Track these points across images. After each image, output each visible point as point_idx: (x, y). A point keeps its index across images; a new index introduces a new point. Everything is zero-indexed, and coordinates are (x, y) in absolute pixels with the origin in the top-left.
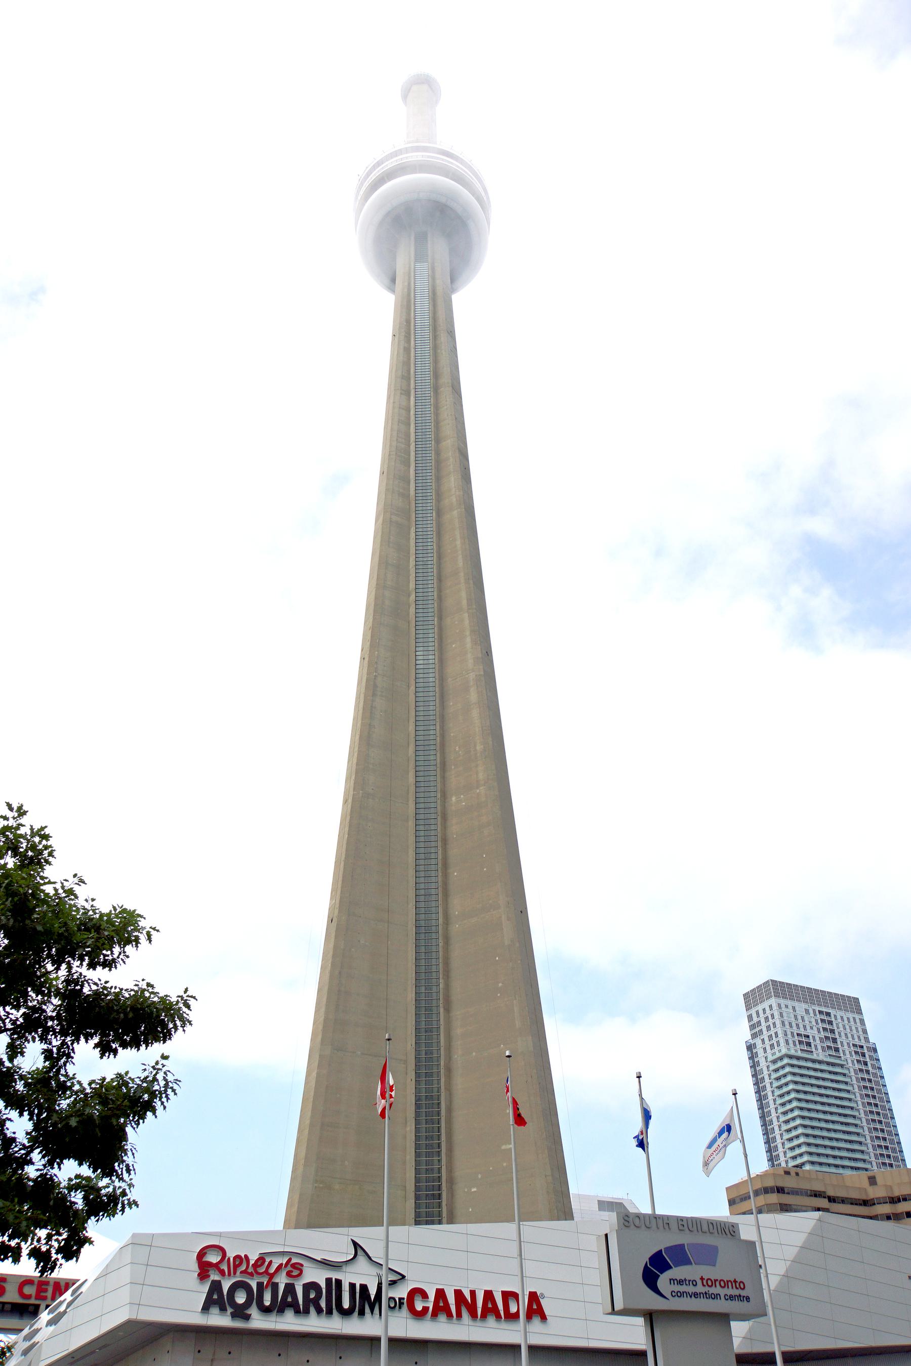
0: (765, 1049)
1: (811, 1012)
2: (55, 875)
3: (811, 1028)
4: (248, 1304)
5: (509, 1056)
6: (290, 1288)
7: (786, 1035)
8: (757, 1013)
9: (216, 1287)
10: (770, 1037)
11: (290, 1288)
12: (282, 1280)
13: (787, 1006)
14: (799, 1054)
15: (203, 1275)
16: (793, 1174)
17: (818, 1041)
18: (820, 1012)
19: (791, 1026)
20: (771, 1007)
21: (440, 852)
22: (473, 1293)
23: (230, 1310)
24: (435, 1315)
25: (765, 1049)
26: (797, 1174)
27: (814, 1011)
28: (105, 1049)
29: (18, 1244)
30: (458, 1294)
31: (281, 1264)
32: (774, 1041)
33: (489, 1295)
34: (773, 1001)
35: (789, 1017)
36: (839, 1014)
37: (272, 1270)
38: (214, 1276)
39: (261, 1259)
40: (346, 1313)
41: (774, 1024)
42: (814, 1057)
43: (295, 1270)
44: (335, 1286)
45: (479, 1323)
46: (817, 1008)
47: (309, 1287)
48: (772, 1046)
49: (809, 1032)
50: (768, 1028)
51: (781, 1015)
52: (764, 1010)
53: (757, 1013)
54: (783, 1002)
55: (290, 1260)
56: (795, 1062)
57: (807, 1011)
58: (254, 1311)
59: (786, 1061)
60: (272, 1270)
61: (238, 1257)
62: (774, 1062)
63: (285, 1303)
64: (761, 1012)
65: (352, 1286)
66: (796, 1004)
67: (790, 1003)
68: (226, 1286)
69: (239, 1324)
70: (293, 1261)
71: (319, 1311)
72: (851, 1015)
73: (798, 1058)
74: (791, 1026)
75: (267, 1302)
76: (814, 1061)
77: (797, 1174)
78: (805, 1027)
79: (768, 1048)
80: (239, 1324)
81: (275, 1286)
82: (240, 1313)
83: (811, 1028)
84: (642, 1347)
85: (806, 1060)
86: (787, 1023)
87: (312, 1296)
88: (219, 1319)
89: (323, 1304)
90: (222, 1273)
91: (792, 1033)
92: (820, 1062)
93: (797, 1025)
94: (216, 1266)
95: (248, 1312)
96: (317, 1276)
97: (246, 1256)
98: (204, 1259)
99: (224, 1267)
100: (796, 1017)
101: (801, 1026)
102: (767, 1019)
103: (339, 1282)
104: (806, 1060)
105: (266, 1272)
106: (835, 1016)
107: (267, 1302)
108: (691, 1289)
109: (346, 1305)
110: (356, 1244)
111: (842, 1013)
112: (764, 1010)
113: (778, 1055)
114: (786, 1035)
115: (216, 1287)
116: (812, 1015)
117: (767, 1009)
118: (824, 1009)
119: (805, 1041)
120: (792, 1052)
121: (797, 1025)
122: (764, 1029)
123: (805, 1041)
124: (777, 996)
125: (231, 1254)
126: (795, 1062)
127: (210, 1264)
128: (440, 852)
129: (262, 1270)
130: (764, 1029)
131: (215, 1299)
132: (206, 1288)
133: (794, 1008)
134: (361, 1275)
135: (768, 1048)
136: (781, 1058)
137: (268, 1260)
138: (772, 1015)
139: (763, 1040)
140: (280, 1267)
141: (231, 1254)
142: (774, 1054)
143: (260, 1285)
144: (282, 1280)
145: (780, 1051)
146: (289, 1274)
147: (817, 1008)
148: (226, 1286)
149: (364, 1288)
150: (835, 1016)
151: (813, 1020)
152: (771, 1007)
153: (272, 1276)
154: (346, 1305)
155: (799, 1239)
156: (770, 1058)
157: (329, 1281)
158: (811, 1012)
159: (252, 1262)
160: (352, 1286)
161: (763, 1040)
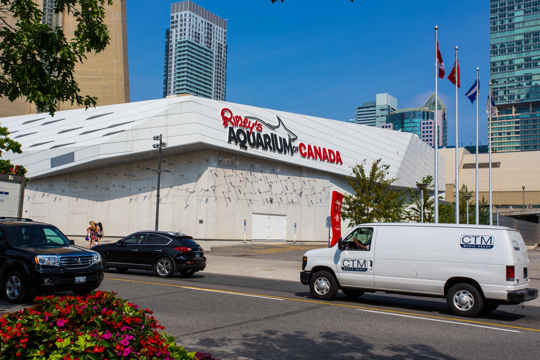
0: (176, 36)
1: (204, 22)
3: (202, 30)
5: (456, 49)
7: (190, 31)
8: (177, 16)
10: (181, 30)
11: (259, 135)
13: (193, 17)
14: (193, 42)
15: (226, 125)
17: (203, 38)
18: (208, 24)
19: (193, 27)
20: (185, 15)
22: (319, 148)
25: (176, 36)
27: (205, 22)
32: (183, 32)
34: (188, 12)
35: (193, 22)
36: (216, 27)
40: (280, 151)
41: (185, 24)
42: (200, 45)
44: (274, 136)
45: (322, 162)
46: (207, 21)
48: (181, 35)
49: (200, 32)
50: (181, 25)
51: (190, 20)
52: (181, 15)
53: (177, 16)
54: (192, 14)
55: (256, 122)
56: (190, 45)
57: (202, 21)
59: (187, 44)
61: (237, 116)
62: (180, 43)
63: (256, 144)
64: (179, 16)
66: (198, 17)
67: (195, 15)
68: (235, 130)
69: (242, 150)
70: (258, 122)
72: (221, 29)
73: (193, 44)
74: (193, 27)
76: (199, 47)
78: (199, 29)
79: (179, 35)
80: (242, 150)
81: (253, 133)
82: (243, 145)
83: (202, 30)
84: (76, 159)
85: (196, 45)
86: (191, 25)
87: (267, 141)
88: (235, 147)
91: (193, 31)
92: (202, 48)
93: (196, 27)
99: (233, 120)
100: (196, 23)
101: (198, 28)
102: (182, 20)
103: (275, 136)
104: (196, 45)
106: (214, 27)
111: (218, 27)
112: (181, 15)
113: (183, 40)
114: (190, 31)
116: (204, 24)
117: (183, 15)
118: (210, 23)
119: (197, 36)
120: (190, 40)
121: (196, 27)
122: (179, 25)
123: (197, 36)
124: (190, 10)
125: (234, 115)
126: (190, 45)
130: (179, 25)
131: (233, 138)
132: (228, 130)
133: (196, 18)
134: (281, 133)
135: (179, 35)
136: (184, 42)
137: (249, 120)
138: (185, 19)
139: (177, 31)
140: (253, 125)
141: (234, 115)
142: (181, 39)
143: (248, 132)
145: (184, 38)
147: (207, 21)
148: (235, 130)
149: (284, 139)
150: (214, 27)
151: (204, 27)
152: (185, 15)
153: (252, 128)
155: (407, 143)
156: (179, 41)
157: (272, 134)
158: (204, 22)
161: (177, 31)
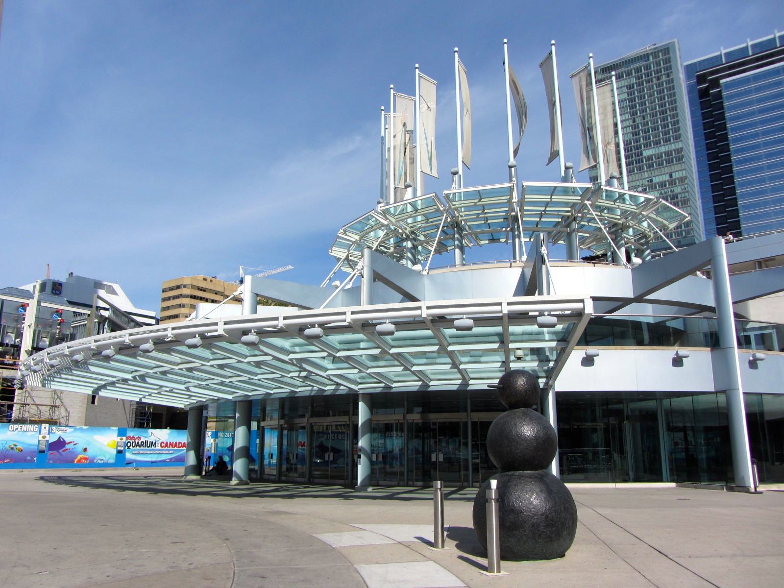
2: (456, 542)
6: (138, 442)
11: (138, 442)
12: (137, 441)
16: (209, 280)
21: (637, 65)
22: (173, 443)
26: (211, 281)
28: (124, 341)
29: (284, 425)
30: (170, 443)
33: (176, 443)
58: (131, 447)
65: (150, 442)
75: (134, 445)
77: (211, 281)
81: (135, 442)
89: (144, 445)
107: (134, 445)
108: (165, 452)
109: (148, 445)
128: (637, 65)
143: (133, 442)
144: (137, 441)
149: (152, 442)
154: (148, 445)
157: (146, 441)
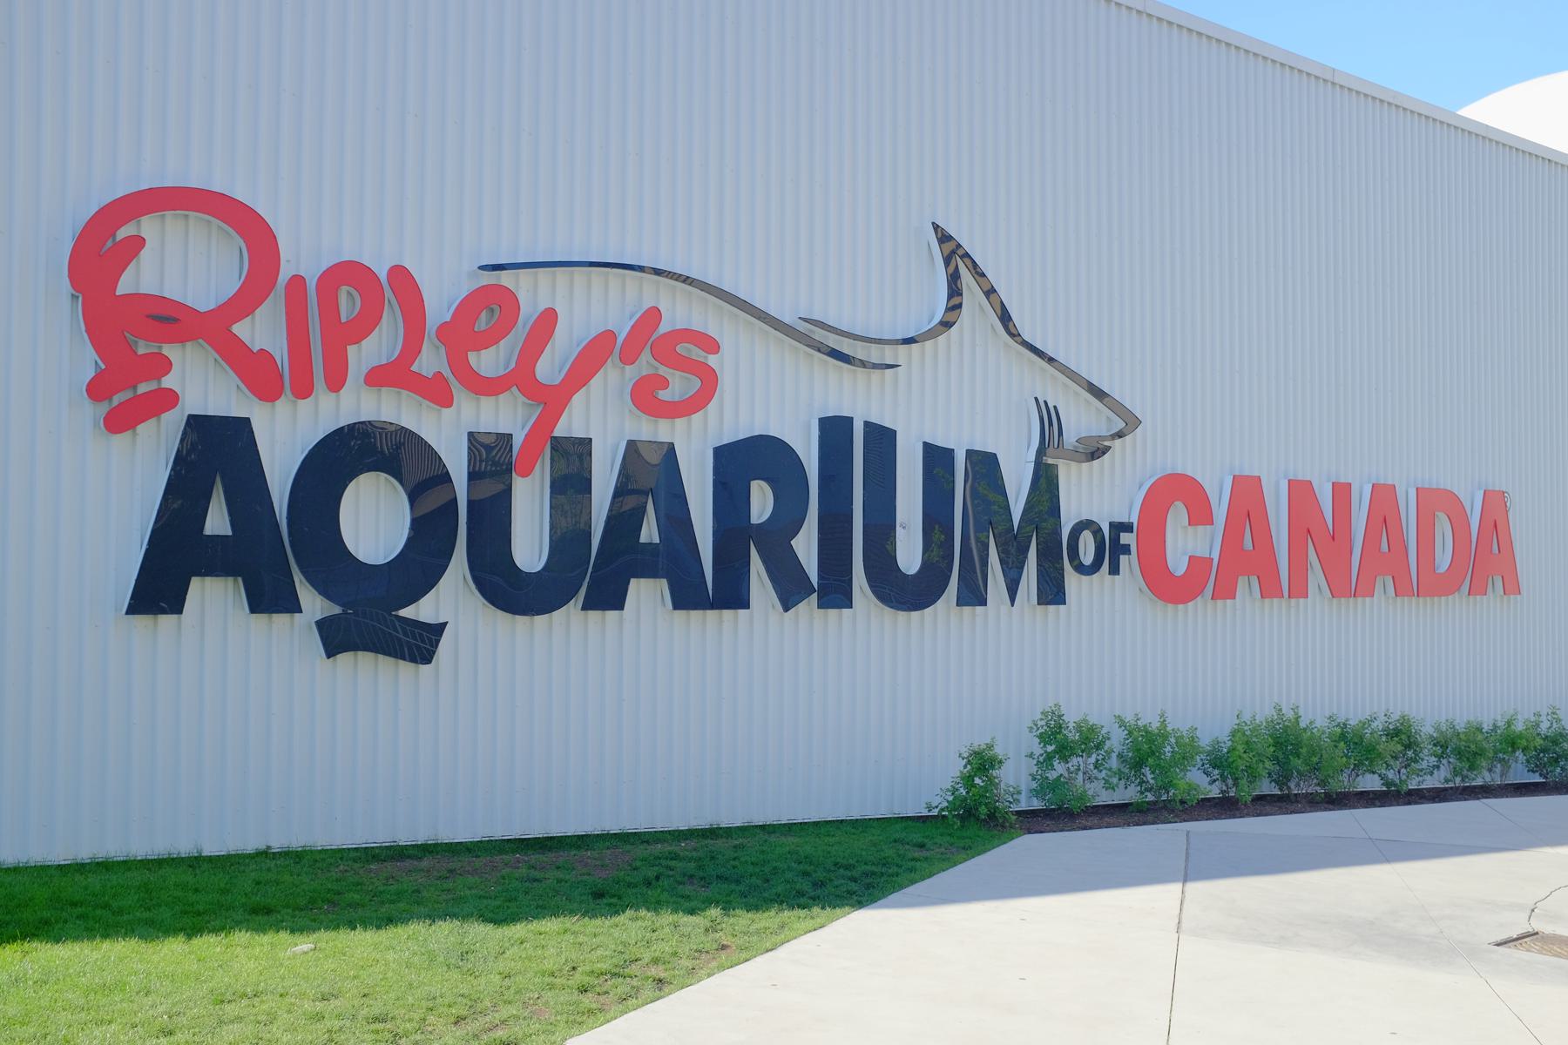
4: (419, 566)
9: (216, 451)
22: (1342, 492)
23: (314, 604)
24: (1225, 591)
30: (1300, 492)
31: (608, 337)
37: (549, 368)
38: (201, 385)
39: (488, 308)
43: (667, 359)
47: (743, 461)
60: (549, 368)
65: (937, 459)
71: (791, 589)
75: (530, 548)
81: (571, 465)
89: (806, 546)
90: (260, 376)
94: (213, 329)
95: (423, 610)
96: (774, 397)
97: (400, 275)
98: (125, 286)
103: (882, 440)
105: (520, 378)
107: (530, 548)
109: (909, 554)
110: (952, 252)
115: (216, 451)
125: (302, 256)
127: (170, 320)
129: (487, 362)
134: (953, 402)
141: (302, 256)
146: (646, 397)
149: (985, 465)
153: (552, 400)
154: (909, 554)
157: (835, 431)
159: (439, 304)
160: (937, 459)
